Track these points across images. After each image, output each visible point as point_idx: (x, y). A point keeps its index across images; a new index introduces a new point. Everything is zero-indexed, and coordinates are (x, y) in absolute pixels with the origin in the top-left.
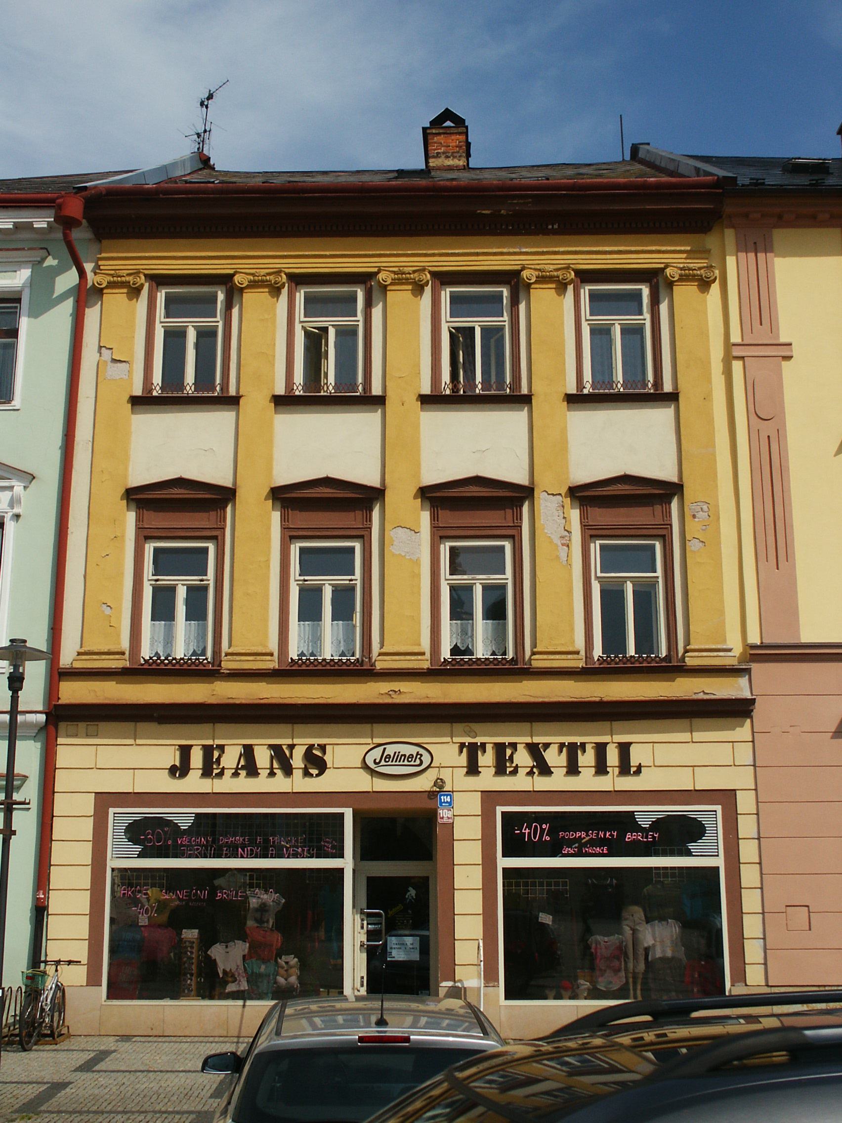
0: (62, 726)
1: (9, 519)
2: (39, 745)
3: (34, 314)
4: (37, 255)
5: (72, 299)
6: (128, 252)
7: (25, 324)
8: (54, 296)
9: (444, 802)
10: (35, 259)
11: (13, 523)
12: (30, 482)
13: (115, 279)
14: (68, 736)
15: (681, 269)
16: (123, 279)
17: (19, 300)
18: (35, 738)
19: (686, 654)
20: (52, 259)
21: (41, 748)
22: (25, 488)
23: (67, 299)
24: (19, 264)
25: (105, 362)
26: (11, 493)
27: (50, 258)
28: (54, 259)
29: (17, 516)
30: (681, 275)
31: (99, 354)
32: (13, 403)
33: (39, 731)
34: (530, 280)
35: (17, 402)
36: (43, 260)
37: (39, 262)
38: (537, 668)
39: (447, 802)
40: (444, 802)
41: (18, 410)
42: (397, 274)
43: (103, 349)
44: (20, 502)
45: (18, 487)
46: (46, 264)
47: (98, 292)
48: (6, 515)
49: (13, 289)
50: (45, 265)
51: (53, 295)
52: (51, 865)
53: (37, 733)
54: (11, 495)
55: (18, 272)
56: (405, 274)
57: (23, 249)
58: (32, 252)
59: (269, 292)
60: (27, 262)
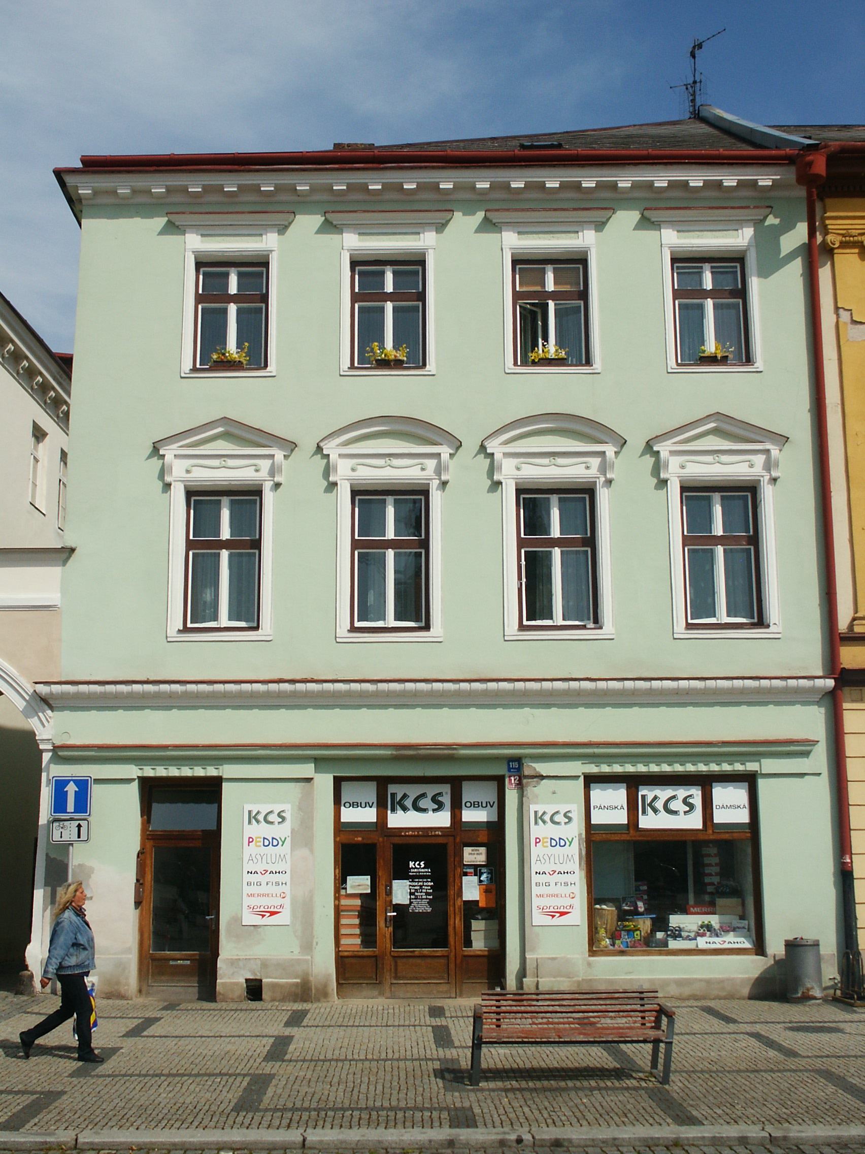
0: (846, 690)
1: (766, 481)
2: (823, 710)
3: (765, 272)
4: (757, 214)
5: (800, 258)
6: (855, 211)
7: (755, 285)
8: (781, 256)
9: (513, 768)
10: (756, 218)
11: (770, 487)
12: (292, 450)
13: (847, 238)
14: (853, 701)
15: (843, 235)
16: (856, 238)
17: (266, 264)
18: (818, 703)
19: (855, 622)
20: (773, 218)
21: (826, 714)
22: (780, 450)
23: (795, 259)
24: (739, 224)
25: (845, 323)
26: (271, 461)
27: (771, 216)
28: (776, 217)
29: (444, 484)
30: (841, 242)
31: (835, 316)
32: (756, 365)
33: (823, 695)
34: (834, 244)
35: (431, 366)
36: (765, 218)
37: (761, 220)
38: (859, 633)
39: (515, 768)
40: (513, 768)
41: (761, 372)
42: (845, 237)
43: (841, 310)
44: (778, 466)
45: (279, 455)
46: (767, 223)
47: (829, 252)
48: (762, 479)
49: (736, 249)
50: (767, 223)
51: (780, 254)
52: (850, 830)
53: (820, 699)
54: (161, 465)
55: (740, 231)
56: (853, 237)
57: (748, 207)
58: (757, 211)
59: (858, 253)
60: (748, 220)
